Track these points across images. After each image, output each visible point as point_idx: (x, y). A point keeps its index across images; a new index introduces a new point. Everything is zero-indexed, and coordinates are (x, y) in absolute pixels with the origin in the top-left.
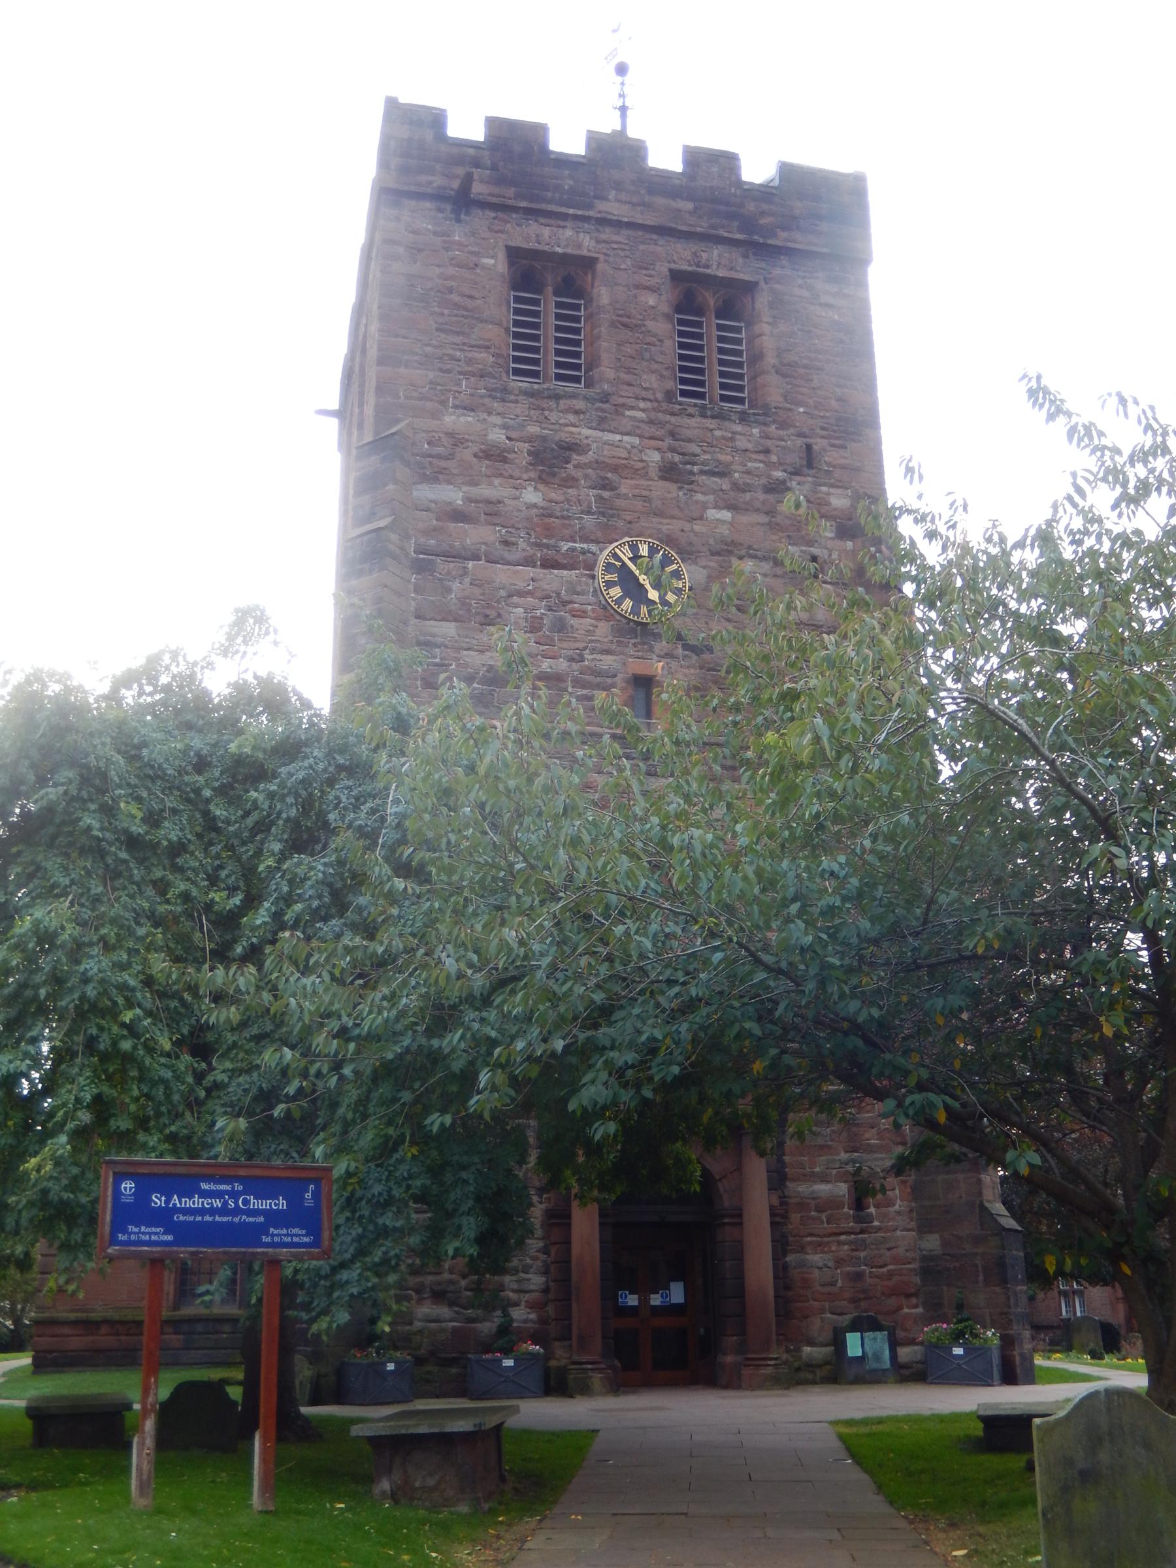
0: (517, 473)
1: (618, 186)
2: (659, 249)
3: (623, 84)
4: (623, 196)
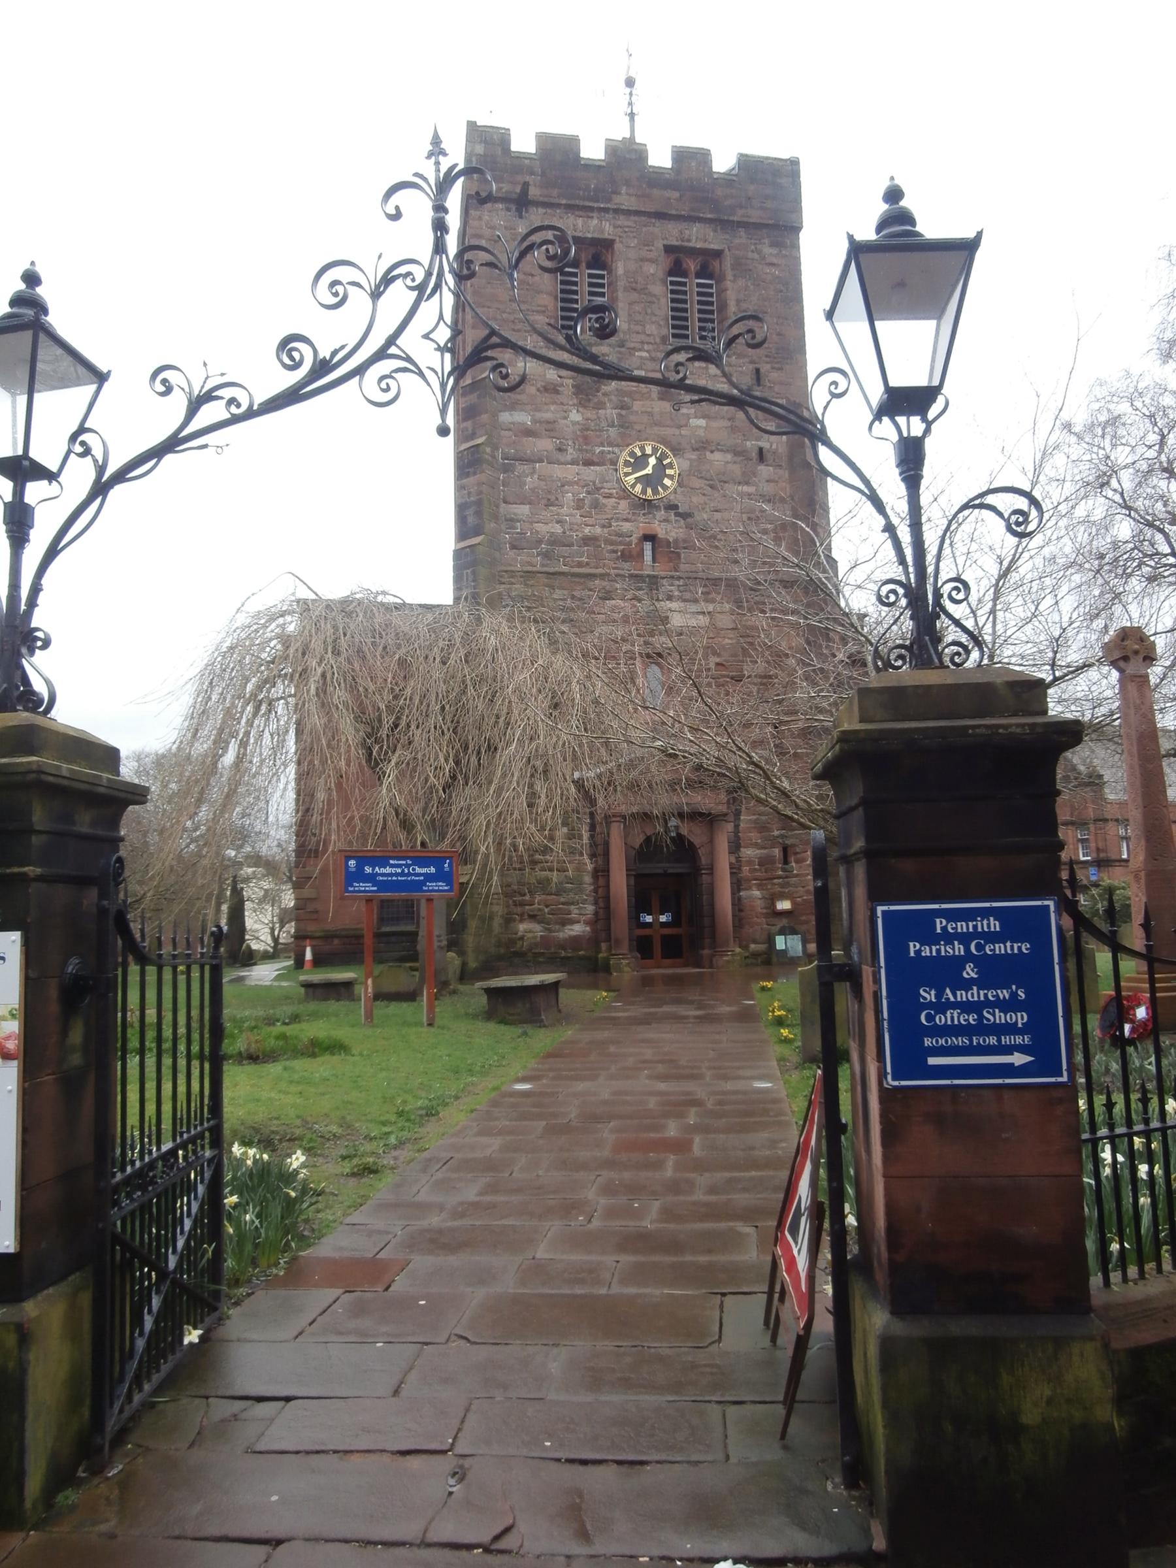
0: (565, 401)
1: (627, 183)
2: (656, 230)
3: (631, 94)
4: (631, 191)
